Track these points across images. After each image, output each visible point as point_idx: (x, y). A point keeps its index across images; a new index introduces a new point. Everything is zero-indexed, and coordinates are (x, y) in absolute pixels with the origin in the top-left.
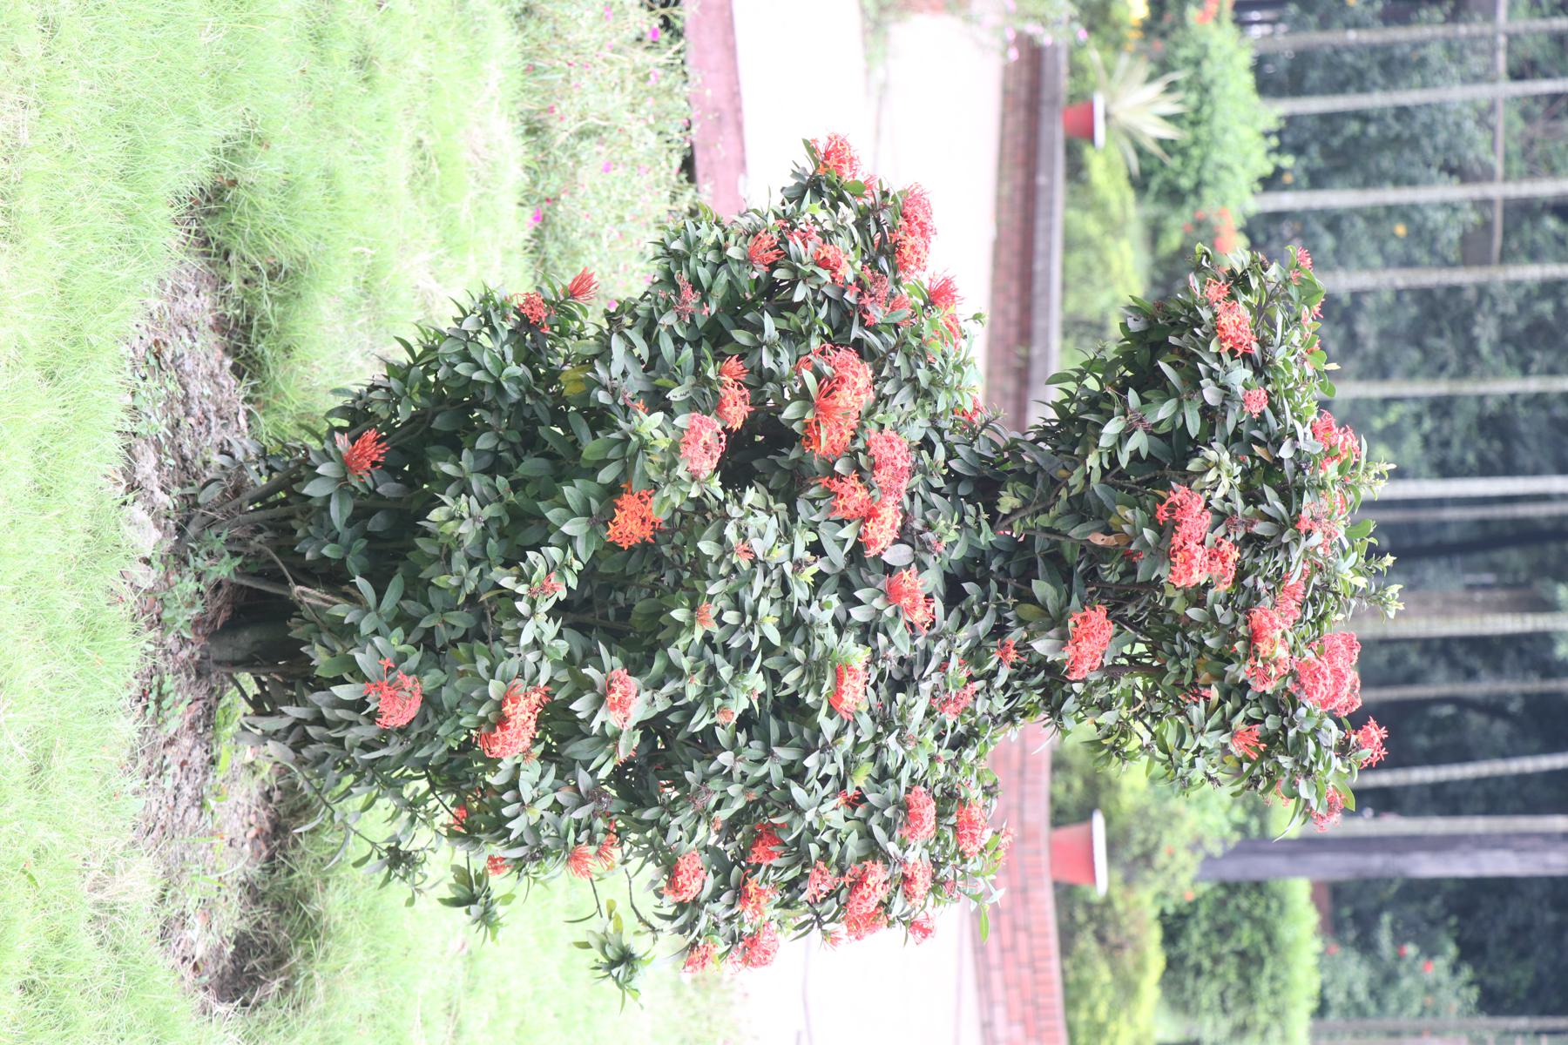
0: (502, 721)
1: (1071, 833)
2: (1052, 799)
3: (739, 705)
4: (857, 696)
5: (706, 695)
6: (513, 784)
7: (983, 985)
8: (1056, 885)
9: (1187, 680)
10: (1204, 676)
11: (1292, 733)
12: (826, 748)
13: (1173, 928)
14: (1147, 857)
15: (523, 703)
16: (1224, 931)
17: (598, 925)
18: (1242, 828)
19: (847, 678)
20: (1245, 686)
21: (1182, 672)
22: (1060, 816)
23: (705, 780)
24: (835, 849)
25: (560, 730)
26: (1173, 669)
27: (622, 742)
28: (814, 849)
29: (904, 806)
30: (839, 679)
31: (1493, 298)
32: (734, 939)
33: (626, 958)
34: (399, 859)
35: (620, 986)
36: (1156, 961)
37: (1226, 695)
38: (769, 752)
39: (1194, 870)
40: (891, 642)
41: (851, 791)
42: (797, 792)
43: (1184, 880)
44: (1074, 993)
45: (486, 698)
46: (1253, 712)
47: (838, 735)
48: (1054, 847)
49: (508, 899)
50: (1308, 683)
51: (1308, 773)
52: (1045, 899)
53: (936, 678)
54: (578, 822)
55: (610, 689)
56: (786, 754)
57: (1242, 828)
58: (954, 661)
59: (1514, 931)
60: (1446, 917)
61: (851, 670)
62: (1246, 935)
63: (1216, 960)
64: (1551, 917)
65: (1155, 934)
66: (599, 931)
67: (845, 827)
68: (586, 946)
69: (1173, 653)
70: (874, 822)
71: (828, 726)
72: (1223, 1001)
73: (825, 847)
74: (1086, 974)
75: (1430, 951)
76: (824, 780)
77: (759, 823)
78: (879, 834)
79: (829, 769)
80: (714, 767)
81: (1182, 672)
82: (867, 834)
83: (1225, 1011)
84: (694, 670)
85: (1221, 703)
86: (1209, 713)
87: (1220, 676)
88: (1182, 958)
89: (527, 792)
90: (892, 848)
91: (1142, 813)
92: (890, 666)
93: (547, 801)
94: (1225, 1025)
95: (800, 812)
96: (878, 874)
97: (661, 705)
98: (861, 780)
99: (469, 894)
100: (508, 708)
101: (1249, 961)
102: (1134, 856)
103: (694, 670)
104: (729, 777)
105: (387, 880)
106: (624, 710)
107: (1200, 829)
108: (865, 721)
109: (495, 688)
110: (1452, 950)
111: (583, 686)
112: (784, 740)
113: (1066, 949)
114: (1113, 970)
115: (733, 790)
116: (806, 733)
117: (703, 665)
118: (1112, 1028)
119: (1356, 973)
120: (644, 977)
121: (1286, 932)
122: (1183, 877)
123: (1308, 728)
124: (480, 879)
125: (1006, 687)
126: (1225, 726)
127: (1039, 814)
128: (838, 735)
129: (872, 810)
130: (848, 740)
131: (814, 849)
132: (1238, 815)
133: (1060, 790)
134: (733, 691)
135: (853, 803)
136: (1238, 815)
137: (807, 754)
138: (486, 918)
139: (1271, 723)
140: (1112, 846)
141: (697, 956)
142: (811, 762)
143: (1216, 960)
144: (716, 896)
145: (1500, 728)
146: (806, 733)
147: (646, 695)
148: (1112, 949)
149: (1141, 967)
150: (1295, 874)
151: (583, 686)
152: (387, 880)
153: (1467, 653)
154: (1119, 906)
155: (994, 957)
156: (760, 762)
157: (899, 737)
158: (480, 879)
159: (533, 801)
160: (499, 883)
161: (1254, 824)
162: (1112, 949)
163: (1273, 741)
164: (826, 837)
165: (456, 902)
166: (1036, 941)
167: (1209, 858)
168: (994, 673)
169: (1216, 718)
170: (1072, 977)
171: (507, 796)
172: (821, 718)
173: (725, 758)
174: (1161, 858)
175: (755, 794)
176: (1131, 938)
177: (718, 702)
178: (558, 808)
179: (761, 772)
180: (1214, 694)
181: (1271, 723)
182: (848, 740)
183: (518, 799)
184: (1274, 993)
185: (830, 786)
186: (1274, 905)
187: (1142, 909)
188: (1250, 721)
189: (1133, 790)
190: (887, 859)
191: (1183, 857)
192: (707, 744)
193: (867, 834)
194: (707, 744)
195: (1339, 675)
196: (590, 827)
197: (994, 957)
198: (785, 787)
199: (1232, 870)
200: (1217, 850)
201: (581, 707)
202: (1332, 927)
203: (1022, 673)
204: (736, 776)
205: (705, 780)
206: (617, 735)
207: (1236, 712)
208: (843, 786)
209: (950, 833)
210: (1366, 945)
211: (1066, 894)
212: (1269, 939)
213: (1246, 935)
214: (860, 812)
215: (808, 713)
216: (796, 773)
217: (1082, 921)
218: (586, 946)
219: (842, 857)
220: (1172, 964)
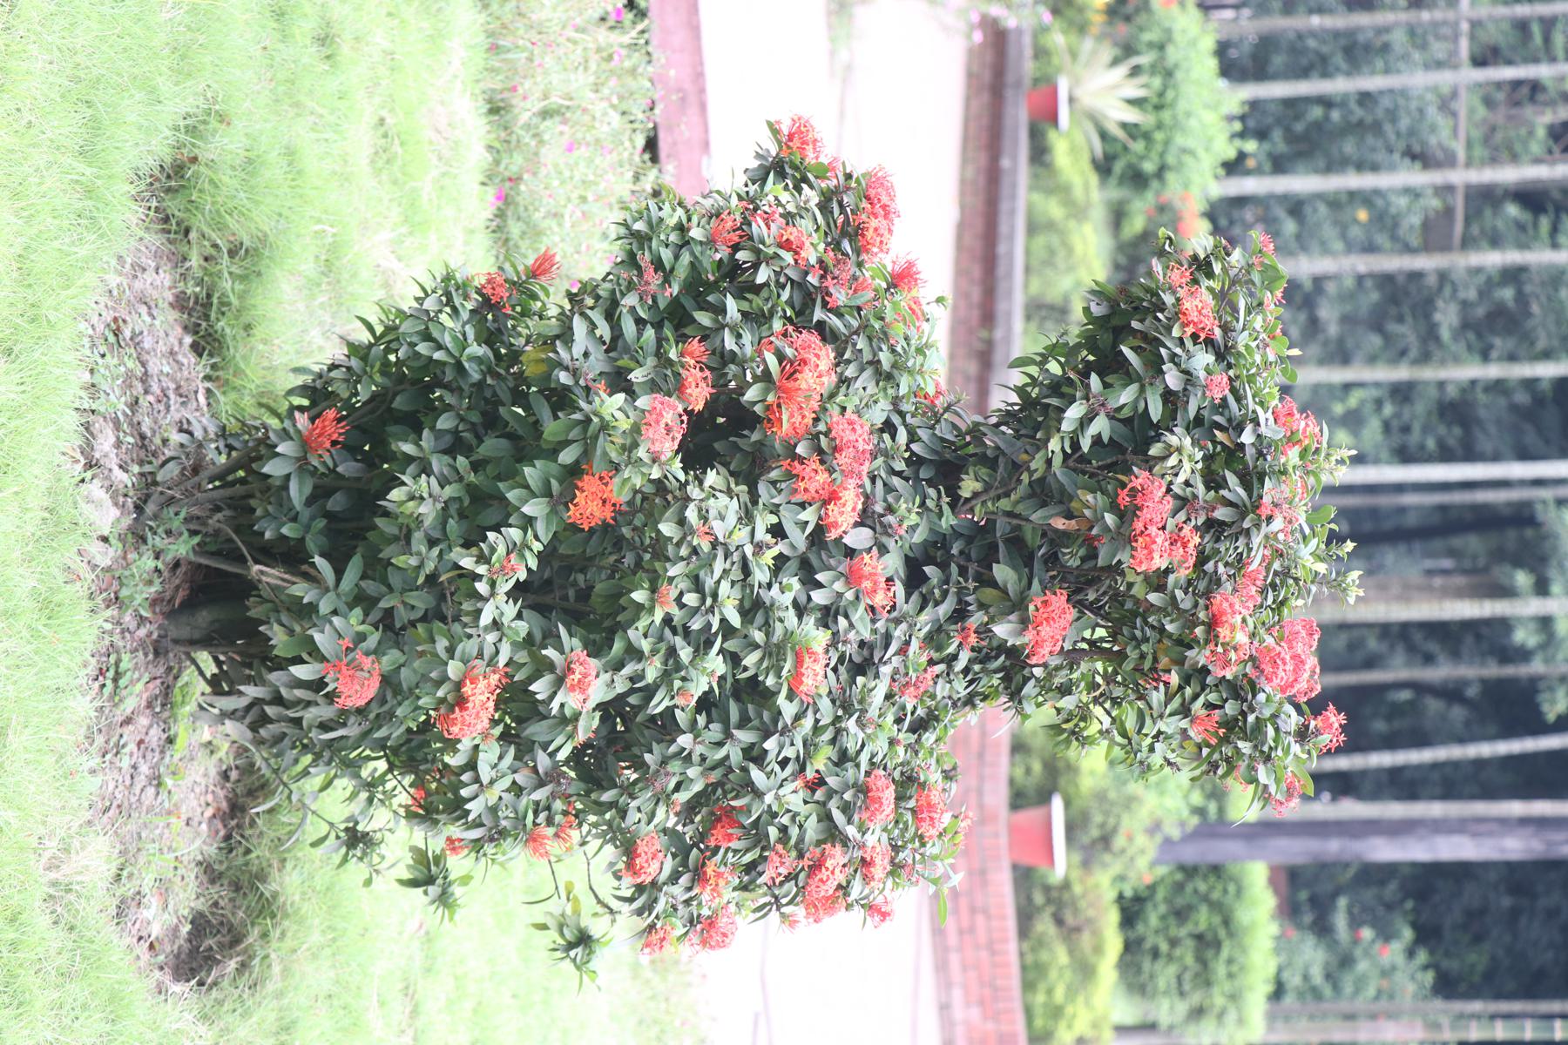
0: (461, 702)
1: (1030, 816)
2: (1012, 782)
4: (817, 679)
5: (666, 677)
6: (472, 765)
7: (941, 967)
8: (1015, 867)
9: (1147, 665)
10: (1164, 661)
11: (1251, 718)
12: (785, 730)
13: (1131, 910)
14: (1105, 841)
15: (482, 684)
16: (1181, 914)
17: (556, 906)
18: (1200, 811)
19: (807, 661)
20: (1205, 671)
21: (1143, 656)
22: (1019, 799)
23: (664, 762)
24: (794, 832)
26: (1133, 654)
27: (582, 723)
28: (773, 832)
29: (863, 790)
30: (799, 662)
33: (584, 939)
34: (356, 839)
37: (1186, 680)
38: (728, 735)
40: (851, 625)
41: (810, 774)
42: (756, 775)
43: (1142, 863)
44: (1032, 975)
45: (444, 679)
46: (1213, 697)
48: (1013, 830)
49: (466, 880)
50: (1268, 669)
51: (1268, 759)
54: (537, 803)
56: (745, 736)
57: (1200, 811)
60: (1402, 901)
61: (811, 653)
62: (1203, 919)
63: (1174, 943)
66: (557, 912)
68: (544, 927)
69: (1134, 638)
70: (833, 806)
71: (788, 709)
73: (784, 830)
74: (1044, 956)
75: (1386, 935)
76: (784, 763)
77: (717, 803)
79: (789, 752)
80: (673, 749)
81: (1143, 656)
82: (826, 817)
83: (1182, 994)
85: (1181, 688)
86: (1169, 698)
87: (1180, 662)
90: (851, 831)
91: (1101, 796)
92: (851, 649)
93: (506, 783)
94: (1182, 1008)
95: (759, 794)
96: (837, 857)
97: (621, 687)
99: (427, 874)
100: (467, 689)
101: (1206, 944)
102: (1093, 841)
103: (654, 652)
105: (345, 860)
106: (583, 691)
108: (825, 704)
109: (454, 669)
110: (1408, 934)
112: (744, 723)
113: (1024, 931)
114: (1071, 952)
115: (692, 772)
116: (766, 715)
117: (663, 647)
118: (1069, 1010)
119: (1313, 956)
120: (602, 959)
121: (1243, 916)
122: (1140, 860)
123: (1267, 713)
124: (438, 860)
125: (966, 671)
126: (1185, 711)
127: (998, 797)
129: (831, 793)
130: (808, 723)
131: (773, 832)
133: (1019, 772)
134: (693, 673)
136: (1197, 798)
137: (767, 735)
139: (1231, 708)
140: (1070, 829)
141: (654, 937)
142: (771, 744)
143: (1174, 943)
144: (674, 878)
145: (1458, 713)
146: (766, 715)
148: (1069, 932)
149: (1098, 949)
150: (1252, 858)
152: (345, 860)
154: (1077, 889)
155: (953, 939)
156: (720, 744)
157: (858, 721)
158: (438, 860)
159: (492, 782)
160: (458, 865)
162: (1069, 932)
164: (785, 820)
165: (414, 883)
167: (1168, 842)
168: (955, 657)
171: (465, 777)
172: (781, 700)
173: (685, 740)
174: (1119, 841)
175: (715, 776)
176: (1089, 921)
177: (677, 684)
178: (516, 789)
180: (1174, 679)
181: (1231, 708)
182: (808, 723)
183: (477, 780)
184: (1230, 976)
185: (789, 769)
186: (1232, 888)
187: (1100, 892)
188: (1210, 706)
189: (1092, 773)
190: (845, 841)
191: (1141, 840)
192: (666, 726)
193: (826, 817)
194: (666, 726)
195: (1298, 661)
196: (548, 808)
197: (953, 939)
198: (745, 770)
202: (1289, 910)
203: (982, 657)
204: (696, 758)
205: (664, 762)
206: (576, 717)
207: (1195, 697)
208: (803, 769)
209: (909, 817)
210: (1322, 929)
211: (1024, 877)
212: (1227, 922)
213: (1203, 919)
214: (819, 795)
216: (755, 755)
217: (1040, 903)
219: (801, 840)
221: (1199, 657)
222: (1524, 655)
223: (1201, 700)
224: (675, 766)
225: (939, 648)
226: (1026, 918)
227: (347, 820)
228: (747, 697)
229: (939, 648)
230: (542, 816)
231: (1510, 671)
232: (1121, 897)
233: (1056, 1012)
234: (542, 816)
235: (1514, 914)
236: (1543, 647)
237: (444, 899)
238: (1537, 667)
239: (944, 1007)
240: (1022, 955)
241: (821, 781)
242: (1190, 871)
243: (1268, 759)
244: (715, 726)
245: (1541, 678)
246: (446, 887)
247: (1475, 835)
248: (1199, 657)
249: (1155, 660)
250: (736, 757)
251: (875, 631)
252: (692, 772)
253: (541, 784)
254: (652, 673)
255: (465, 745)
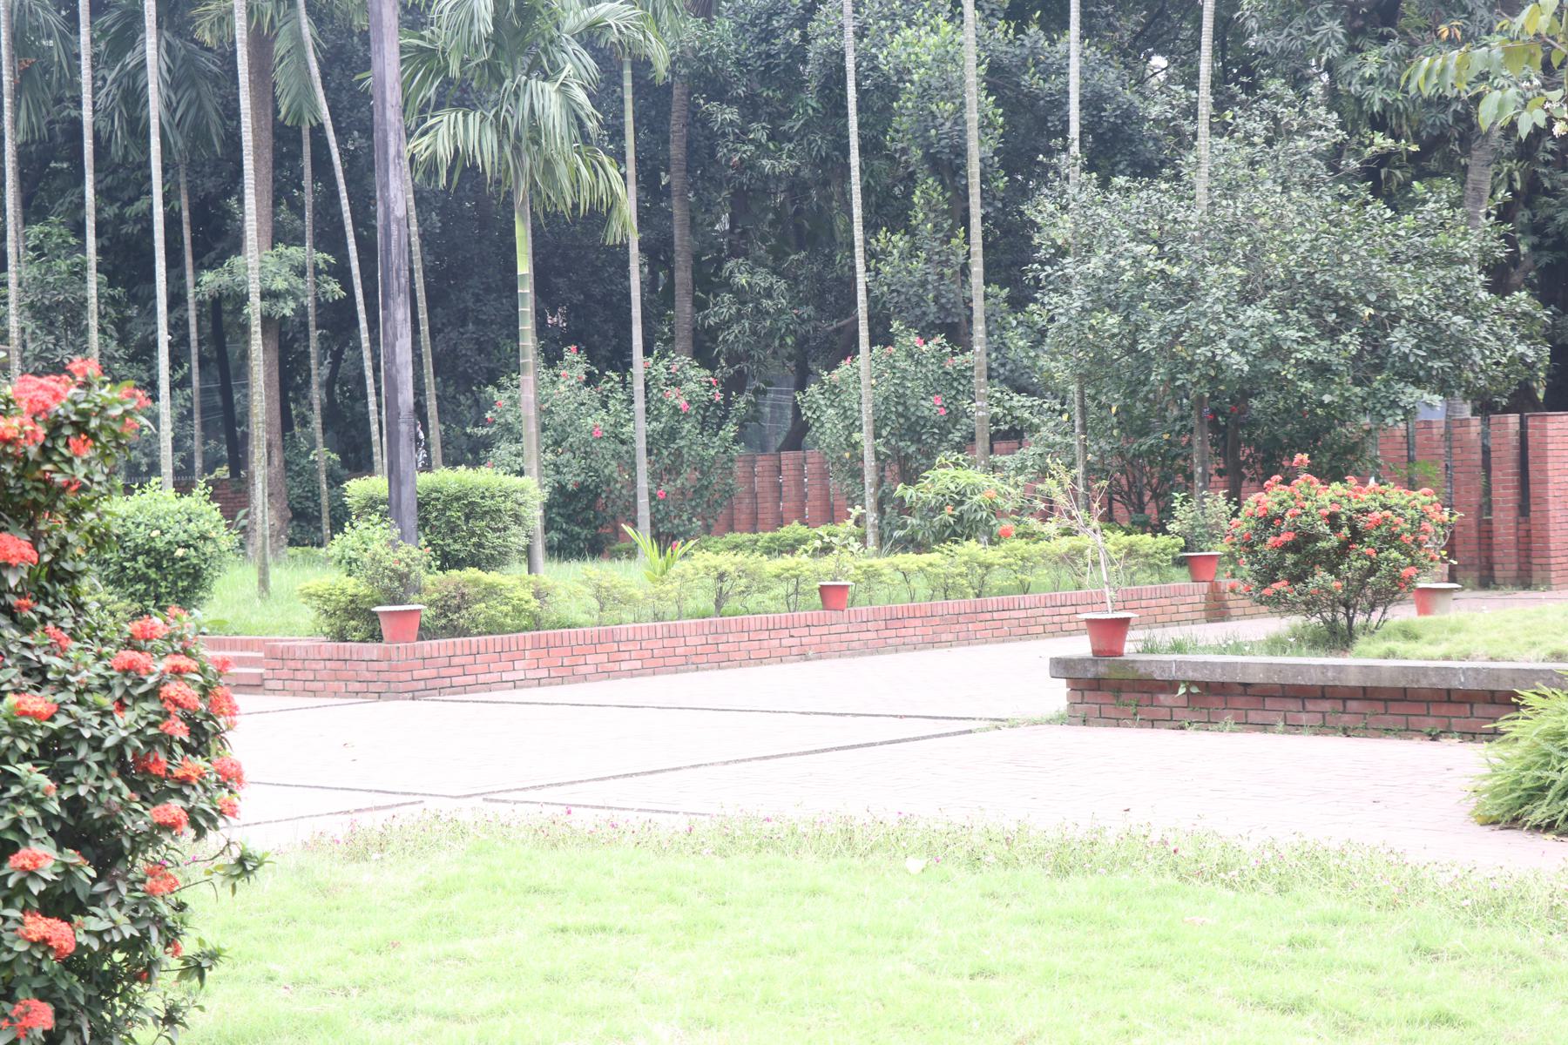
0: (45, 941)
1: (385, 626)
2: (363, 641)
3: (45, 781)
4: (38, 702)
5: (35, 803)
6: (99, 935)
7: (488, 686)
8: (421, 638)
9: (41, 486)
10: (38, 475)
11: (74, 418)
12: (79, 723)
13: (449, 561)
14: (402, 577)
15: (31, 927)
16: (453, 529)
17: (217, 879)
18: (383, 515)
19: (24, 708)
20: (43, 448)
21: (37, 489)
22: (375, 636)
23: (100, 804)
24: (152, 718)
25: (62, 902)
26: (33, 495)
27: (68, 860)
28: (151, 731)
29: (125, 672)
30: (25, 714)
31: (42, 351)
32: (221, 785)
33: (241, 861)
34: (171, 1018)
35: (261, 864)
36: (471, 573)
37: (50, 460)
38: (81, 762)
39: (411, 547)
40: (10, 681)
41: (112, 708)
42: (109, 743)
43: (416, 553)
44: (493, 627)
45: (28, 953)
46: (61, 443)
47: (69, 715)
48: (394, 639)
49: (201, 942)
50: (40, 406)
51: (103, 408)
52: (428, 646)
53: (38, 652)
54: (130, 891)
55: (23, 868)
56: (83, 751)
57: (383, 515)
58: (27, 639)
59: (480, 351)
60: (473, 392)
61: (19, 704)
62: (454, 513)
63: (473, 534)
64: (471, 327)
65: (454, 573)
66: (221, 879)
67: (138, 711)
68: (234, 886)
69: (21, 494)
70: (137, 692)
71: (63, 720)
72: (499, 530)
73: (151, 724)
74: (481, 618)
75: (491, 403)
76: (103, 724)
77: (131, 766)
78: (143, 689)
79: (96, 721)
80: (90, 799)
81: (37, 489)
82: (145, 696)
83: (505, 529)
84: (14, 811)
85: (55, 463)
86: (61, 471)
87: (38, 464)
88: (471, 555)
89: (106, 925)
90: (151, 680)
91: (371, 580)
92: (27, 682)
93: (114, 912)
94: (515, 529)
95: (124, 741)
96: (173, 689)
97: (43, 834)
98: (107, 702)
99: (195, 969)
100: (34, 937)
101: (471, 512)
102: (401, 585)
103: (14, 811)
104: (99, 789)
105: (184, 1024)
106: (39, 858)
107: (383, 542)
108: (60, 697)
109: (20, 947)
110: (490, 389)
111: (22, 887)
112: (74, 752)
113: (465, 632)
114: (478, 601)
115: (107, 785)
116: (68, 737)
117: (12, 805)
118: (515, 602)
119: (504, 450)
120: (256, 847)
121: (453, 488)
122: (414, 554)
123: (71, 407)
124: (186, 961)
125: (54, 608)
126: (69, 461)
127: (373, 649)
128: (69, 715)
129: (127, 693)
130: (73, 708)
131: (151, 731)
132: (375, 518)
133: (358, 635)
134: (31, 784)
135: (121, 705)
136: (375, 518)
137: (81, 736)
138: (214, 956)
139: (67, 431)
140: (394, 602)
141: (227, 810)
142: (87, 734)
143: (473, 534)
144: (186, 798)
145: (347, 353)
146: (68, 737)
147: (31, 843)
148: (464, 602)
149: (476, 582)
150: (414, 482)
151: (22, 887)
152: (184, 1024)
153: (873, 525)
154: (435, 596)
155: (470, 679)
156: (88, 768)
157: (73, 674)
158: (186, 962)
159: (113, 921)
160: (189, 946)
161: (381, 507)
162: (464, 602)
163: (80, 428)
164: (143, 723)
165: (202, 977)
166: (458, 652)
167: (402, 536)
168: (43, 614)
169: (65, 467)
170: (482, 628)
171: (107, 939)
172: (55, 726)
173: (82, 791)
174: (402, 568)
175: (112, 771)
176: (457, 588)
177: (38, 795)
178: (120, 905)
179: (95, 767)
180: (48, 467)
181: (67, 431)
182: (73, 708)
183: (109, 931)
184: (493, 497)
185: (108, 721)
186: (434, 495)
187: (437, 582)
188: (67, 445)
189: (357, 586)
190: (159, 684)
191: (401, 554)
192: (75, 805)
193: (145, 696)
194: (75, 805)
195: (41, 387)
196: (133, 883)
197: (470, 679)
198: (107, 750)
199: (411, 521)
200: (397, 531)
201: (36, 888)
202: (476, 463)
203: (42, 595)
204: (98, 784)
205: (100, 804)
206: (65, 864)
207: (61, 454)
208: (110, 713)
209: (150, 644)
210: (487, 444)
211: (426, 633)
212: (458, 499)
213: (454, 513)
214: (128, 702)
215: (56, 736)
216: (96, 743)
217: (449, 620)
218: (234, 886)
219: (159, 713)
220: (475, 563)
221: (33, 451)
222: (301, 311)
223: (64, 451)
224: (103, 797)
225: (34, 624)
226: (455, 631)
227: (156, 1024)
228: (55, 752)
229: (34, 624)
230: (138, 886)
231: (311, 319)
232: (441, 568)
233: (518, 611)
234: (138, 886)
235: (478, 322)
236: (296, 298)
237: (214, 956)
238: (309, 302)
239: (515, 685)
240: (480, 634)
241: (120, 700)
242: (424, 523)
243: (103, 408)
244: (76, 771)
245: (317, 299)
246: (205, 956)
247: (395, 338)
248: (33, 451)
249: (39, 480)
250: (99, 756)
251: (14, 666)
252: (107, 785)
253: (116, 889)
254: (31, 812)
255: (83, 939)
